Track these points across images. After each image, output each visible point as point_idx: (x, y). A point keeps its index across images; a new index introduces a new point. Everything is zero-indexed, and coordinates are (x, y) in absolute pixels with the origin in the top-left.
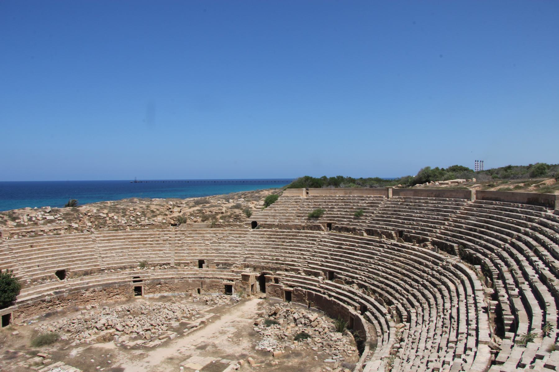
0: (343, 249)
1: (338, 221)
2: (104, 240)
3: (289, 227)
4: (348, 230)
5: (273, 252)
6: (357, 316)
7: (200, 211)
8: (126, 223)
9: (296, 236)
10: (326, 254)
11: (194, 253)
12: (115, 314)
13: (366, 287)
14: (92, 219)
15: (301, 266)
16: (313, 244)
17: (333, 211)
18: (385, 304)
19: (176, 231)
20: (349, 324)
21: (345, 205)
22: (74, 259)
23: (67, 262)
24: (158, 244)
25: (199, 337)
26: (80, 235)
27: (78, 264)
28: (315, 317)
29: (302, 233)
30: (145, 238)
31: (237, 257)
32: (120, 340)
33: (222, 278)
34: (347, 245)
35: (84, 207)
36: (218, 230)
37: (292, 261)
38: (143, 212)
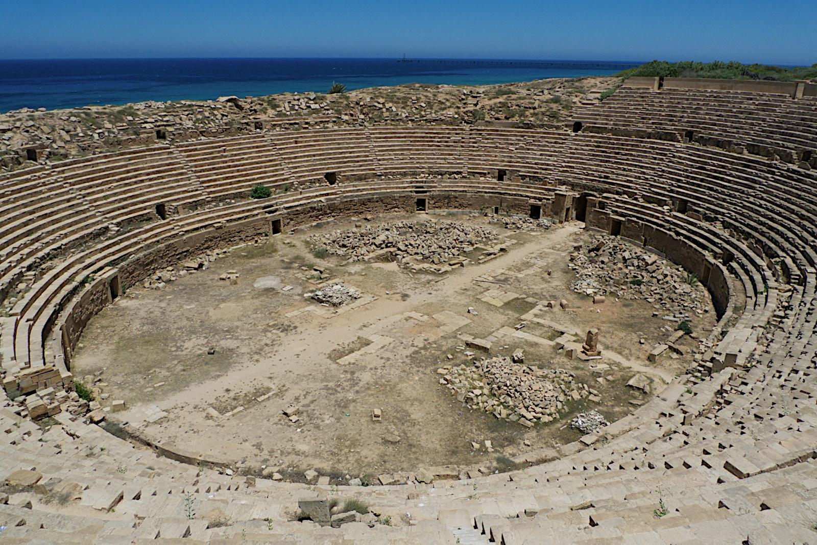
0: (707, 170)
1: (705, 128)
2: (380, 138)
3: (628, 134)
4: (718, 144)
5: (601, 166)
6: (717, 266)
7: (503, 105)
8: (407, 117)
9: (637, 146)
10: (680, 175)
11: (492, 161)
12: (395, 230)
13: (736, 228)
14: (365, 110)
15: (639, 189)
16: (661, 159)
17: (698, 114)
18: (764, 255)
19: (471, 130)
20: (711, 280)
21: (720, 106)
22: (345, 160)
23: (337, 163)
24: (447, 146)
25: (498, 266)
26: (352, 130)
27: (350, 166)
28: (654, 260)
29: (646, 142)
30: (431, 137)
31: (551, 170)
32: (404, 260)
33: (527, 196)
34: (714, 165)
35: (354, 93)
36: (527, 132)
37: (628, 181)
38: (429, 103)
